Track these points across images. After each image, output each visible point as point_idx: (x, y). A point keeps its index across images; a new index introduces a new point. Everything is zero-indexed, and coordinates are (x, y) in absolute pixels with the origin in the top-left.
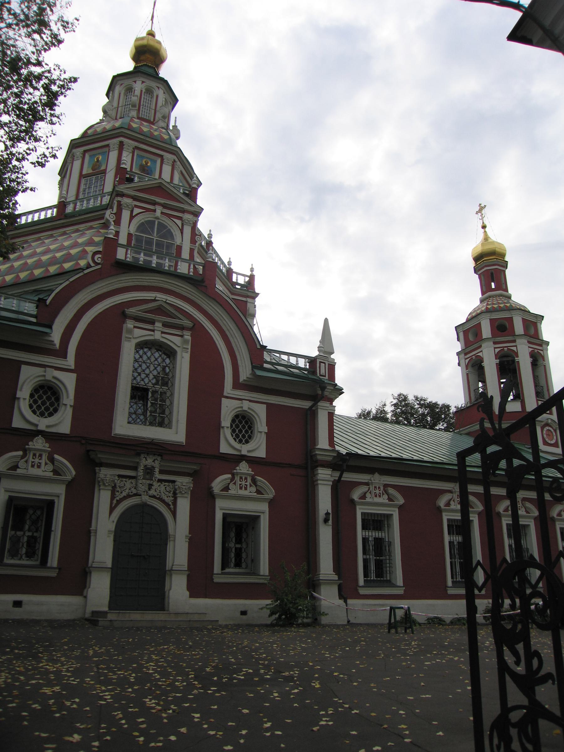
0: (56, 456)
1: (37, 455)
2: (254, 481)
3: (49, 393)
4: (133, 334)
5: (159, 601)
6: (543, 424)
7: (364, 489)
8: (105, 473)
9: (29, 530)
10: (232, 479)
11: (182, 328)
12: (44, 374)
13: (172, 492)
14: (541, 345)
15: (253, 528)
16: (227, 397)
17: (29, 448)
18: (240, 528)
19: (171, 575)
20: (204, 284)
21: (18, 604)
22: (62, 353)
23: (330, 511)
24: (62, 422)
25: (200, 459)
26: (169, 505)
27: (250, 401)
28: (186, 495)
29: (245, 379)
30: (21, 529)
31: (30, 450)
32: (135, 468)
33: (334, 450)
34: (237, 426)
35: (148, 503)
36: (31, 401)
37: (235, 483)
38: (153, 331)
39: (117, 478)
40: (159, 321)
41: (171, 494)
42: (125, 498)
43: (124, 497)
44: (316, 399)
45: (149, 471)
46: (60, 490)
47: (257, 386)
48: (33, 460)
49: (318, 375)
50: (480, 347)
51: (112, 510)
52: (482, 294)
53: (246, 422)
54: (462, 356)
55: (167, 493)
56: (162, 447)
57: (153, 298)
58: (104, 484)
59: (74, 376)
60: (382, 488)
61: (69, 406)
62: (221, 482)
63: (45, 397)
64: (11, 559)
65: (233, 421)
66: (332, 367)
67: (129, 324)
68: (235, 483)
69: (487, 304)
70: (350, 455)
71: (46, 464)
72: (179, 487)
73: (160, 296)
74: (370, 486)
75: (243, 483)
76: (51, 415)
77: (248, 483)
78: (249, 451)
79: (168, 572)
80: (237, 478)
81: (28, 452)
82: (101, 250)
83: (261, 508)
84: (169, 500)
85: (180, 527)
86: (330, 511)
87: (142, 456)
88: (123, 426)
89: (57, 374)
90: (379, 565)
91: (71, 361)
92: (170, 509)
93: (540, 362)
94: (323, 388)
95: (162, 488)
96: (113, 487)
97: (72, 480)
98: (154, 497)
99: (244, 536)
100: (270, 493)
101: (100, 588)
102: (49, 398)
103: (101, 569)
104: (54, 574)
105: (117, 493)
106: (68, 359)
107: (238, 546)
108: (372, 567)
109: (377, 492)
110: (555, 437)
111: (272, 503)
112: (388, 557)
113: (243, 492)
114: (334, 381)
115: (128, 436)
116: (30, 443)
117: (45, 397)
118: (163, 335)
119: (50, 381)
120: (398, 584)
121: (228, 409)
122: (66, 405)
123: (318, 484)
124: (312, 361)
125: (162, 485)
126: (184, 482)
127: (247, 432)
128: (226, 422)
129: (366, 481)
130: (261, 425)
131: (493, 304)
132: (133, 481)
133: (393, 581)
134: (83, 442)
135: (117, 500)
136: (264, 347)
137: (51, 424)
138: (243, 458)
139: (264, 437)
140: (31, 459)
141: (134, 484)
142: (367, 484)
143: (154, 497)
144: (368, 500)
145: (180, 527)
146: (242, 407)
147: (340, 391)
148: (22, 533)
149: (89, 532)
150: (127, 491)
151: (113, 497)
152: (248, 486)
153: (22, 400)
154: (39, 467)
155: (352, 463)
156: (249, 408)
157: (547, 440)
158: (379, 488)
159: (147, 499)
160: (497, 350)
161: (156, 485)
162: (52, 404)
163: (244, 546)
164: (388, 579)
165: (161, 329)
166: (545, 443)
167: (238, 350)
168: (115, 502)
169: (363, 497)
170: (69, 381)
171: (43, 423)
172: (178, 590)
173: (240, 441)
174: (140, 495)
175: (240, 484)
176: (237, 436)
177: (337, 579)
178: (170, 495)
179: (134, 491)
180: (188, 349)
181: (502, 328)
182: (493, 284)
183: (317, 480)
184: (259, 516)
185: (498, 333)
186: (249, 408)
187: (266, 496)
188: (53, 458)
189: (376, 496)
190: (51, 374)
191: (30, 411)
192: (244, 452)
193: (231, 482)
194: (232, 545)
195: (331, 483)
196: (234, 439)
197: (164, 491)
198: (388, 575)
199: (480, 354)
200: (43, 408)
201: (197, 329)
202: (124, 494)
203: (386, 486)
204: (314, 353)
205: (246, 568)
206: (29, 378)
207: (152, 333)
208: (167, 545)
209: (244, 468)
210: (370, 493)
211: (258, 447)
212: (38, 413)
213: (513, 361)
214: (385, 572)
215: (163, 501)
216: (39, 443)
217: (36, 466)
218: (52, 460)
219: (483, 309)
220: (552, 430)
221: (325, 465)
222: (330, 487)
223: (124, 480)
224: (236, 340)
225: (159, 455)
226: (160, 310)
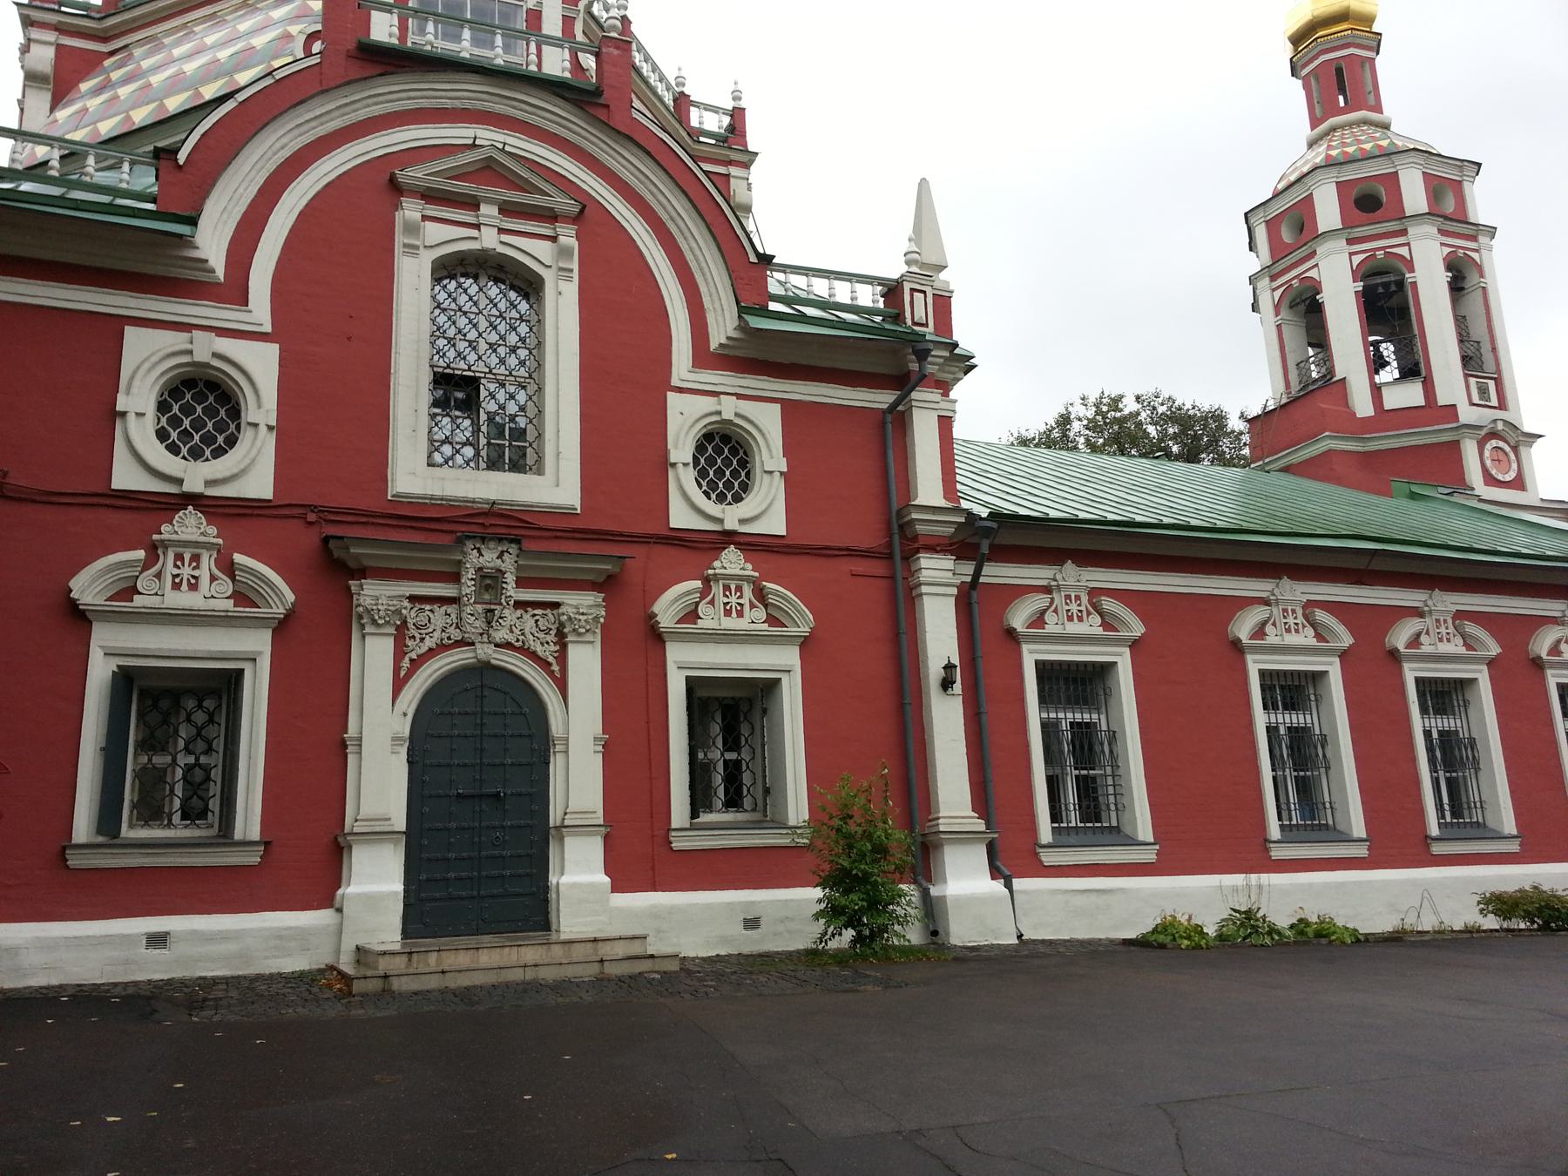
0: (239, 558)
1: (187, 557)
3: (211, 399)
4: (424, 238)
5: (530, 909)
6: (1483, 433)
7: (1039, 601)
8: (374, 594)
9: (188, 751)
10: (706, 591)
11: (551, 217)
12: (189, 347)
13: (553, 632)
14: (1474, 238)
15: (765, 711)
16: (680, 390)
17: (162, 541)
18: (731, 710)
19: (561, 839)
20: (601, 101)
21: (158, 940)
22: (235, 291)
23: (956, 661)
24: (251, 468)
25: (614, 551)
26: (550, 664)
27: (739, 396)
28: (589, 637)
29: (724, 341)
30: (162, 748)
31: (165, 545)
32: (455, 578)
33: (957, 510)
34: (711, 462)
36: (164, 420)
37: (712, 602)
38: (477, 227)
39: (406, 603)
40: (490, 201)
42: (431, 653)
44: (903, 383)
45: (490, 582)
47: (761, 354)
48: (176, 571)
49: (909, 322)
50: (1314, 253)
51: (398, 685)
52: (1313, 127)
53: (734, 451)
54: (1264, 283)
55: (541, 635)
57: (470, 142)
58: (374, 622)
59: (272, 351)
60: (1085, 599)
61: (263, 429)
62: (676, 600)
63: (199, 409)
65: (700, 449)
66: (943, 304)
67: (411, 210)
68: (712, 602)
69: (1330, 147)
70: (995, 515)
71: (213, 578)
72: (570, 618)
73: (487, 136)
74: (1055, 595)
75: (733, 600)
76: (219, 453)
77: (744, 601)
78: (742, 521)
79: (552, 832)
80: (718, 589)
81: (160, 552)
82: (319, 27)
83: (781, 661)
84: (548, 651)
86: (956, 661)
88: (413, 472)
89: (226, 345)
90: (1087, 789)
91: (260, 310)
92: (551, 674)
93: (1472, 279)
94: (922, 355)
96: (398, 628)
97: (287, 616)
98: (508, 645)
99: (745, 730)
100: (803, 622)
101: (377, 880)
102: (211, 412)
103: (378, 836)
104: (253, 858)
105: (410, 643)
106: (251, 306)
107: (731, 756)
108: (1071, 795)
109: (1074, 607)
110: (1515, 466)
112: (1109, 769)
113: (732, 623)
114: (951, 337)
115: (432, 498)
116: (165, 528)
117: (199, 409)
119: (207, 365)
120: (1141, 838)
121: (684, 420)
122: (256, 425)
124: (892, 291)
125: (527, 617)
126: (582, 604)
127: (735, 474)
128: (681, 449)
129: (1044, 583)
130: (771, 456)
131: (1344, 144)
132: (452, 609)
133: (1127, 829)
134: (312, 517)
135: (412, 660)
136: (766, 260)
137: (219, 476)
138: (728, 538)
139: (779, 485)
140: (170, 569)
141: (453, 616)
142: (1047, 590)
143: (508, 645)
144: (1052, 627)
146: (719, 413)
147: (965, 364)
148: (169, 759)
149: (343, 745)
150: (437, 635)
151: (400, 653)
152: (747, 607)
153: (131, 417)
154: (193, 587)
155: (1006, 539)
156: (737, 415)
157: (1493, 472)
158: (1078, 598)
160: (1357, 259)
161: (510, 615)
162: (220, 427)
163: (745, 755)
164: (1114, 823)
165: (496, 222)
166: (1490, 480)
167: (701, 269)
168: (406, 663)
169: (1039, 620)
170: (259, 368)
171: (196, 476)
172: (578, 871)
173: (721, 498)
174: (473, 644)
175: (175, 576)
176: (713, 485)
177: (982, 828)
178: (549, 638)
179: (456, 635)
180: (571, 271)
181: (1369, 203)
182: (1341, 98)
185: (1370, 241)
186: (737, 415)
187: (792, 630)
188: (232, 563)
189: (1070, 619)
190: (204, 348)
191: (161, 448)
192: (731, 524)
193: (702, 598)
194: (716, 754)
195: (955, 591)
196: (705, 493)
197: (534, 630)
198: (1113, 814)
199: (1313, 273)
200: (197, 437)
201: (586, 215)
202: (429, 643)
203: (1094, 593)
204: (894, 269)
205: (754, 810)
206: (146, 361)
207: (474, 233)
209: (731, 562)
210: (1056, 611)
211: (765, 509)
212: (184, 451)
213: (1401, 284)
214: (1103, 807)
215: (533, 656)
217: (185, 586)
218: (229, 569)
219: (1317, 160)
220: (1507, 449)
221: (935, 547)
225: (512, 541)
226: (490, 170)
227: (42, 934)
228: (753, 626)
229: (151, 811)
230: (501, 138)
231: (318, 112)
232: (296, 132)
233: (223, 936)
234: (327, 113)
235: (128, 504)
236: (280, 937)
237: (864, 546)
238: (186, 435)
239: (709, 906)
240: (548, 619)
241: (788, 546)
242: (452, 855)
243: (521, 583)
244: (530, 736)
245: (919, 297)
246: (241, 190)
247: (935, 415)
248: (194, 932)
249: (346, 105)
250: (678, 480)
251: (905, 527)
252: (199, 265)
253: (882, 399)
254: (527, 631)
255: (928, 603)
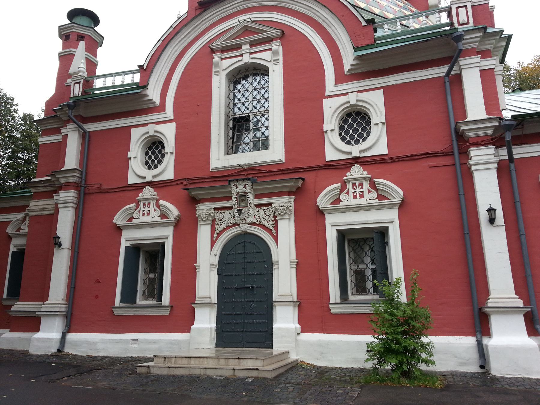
2: (373, 185)
5: (264, 338)
8: (203, 209)
11: (269, 40)
13: (272, 216)
16: (330, 97)
17: (347, 179)
18: (364, 244)
21: (135, 342)
22: (162, 108)
24: (167, 170)
31: (348, 181)
35: (248, 231)
36: (147, 157)
38: (241, 55)
39: (213, 211)
40: (245, 43)
41: (271, 218)
42: (225, 229)
43: (224, 228)
44: (451, 59)
46: (168, 232)
47: (370, 68)
48: (354, 191)
55: (267, 218)
56: (255, 169)
61: (380, 125)
64: (152, 300)
67: (216, 58)
68: (348, 193)
73: (242, 18)
78: (361, 151)
80: (350, 186)
83: (389, 218)
85: (284, 251)
87: (232, 184)
92: (272, 234)
95: (262, 213)
100: (397, 194)
101: (206, 321)
104: (167, 312)
111: (402, 206)
116: (140, 195)
118: (252, 56)
119: (153, 136)
121: (331, 111)
123: (472, 171)
132: (230, 211)
135: (218, 233)
138: (356, 160)
140: (351, 191)
141: (232, 214)
145: (284, 251)
151: (213, 230)
154: (362, 196)
159: (246, 227)
161: (253, 211)
165: (248, 51)
168: (215, 235)
171: (355, 151)
172: (285, 321)
174: (239, 225)
176: (361, 135)
178: (270, 219)
183: (471, 166)
184: (387, 228)
187: (392, 201)
188: (374, 182)
190: (151, 130)
195: (496, 165)
201: (285, 34)
202: (223, 226)
207: (240, 58)
208: (272, 274)
211: (377, 143)
212: (353, 142)
215: (264, 227)
216: (148, 192)
217: (146, 214)
221: (480, 143)
222: (495, 171)
223: (222, 211)
224: (333, 28)
226: (246, 30)
227: (103, 338)
228: (370, 202)
229: (361, 289)
230: (248, 17)
231: (185, 34)
232: (179, 44)
233: (155, 342)
234: (189, 33)
235: (134, 188)
236: (171, 343)
237: (436, 151)
238: (352, 137)
239: (348, 343)
240: (269, 211)
241: (389, 159)
242: (234, 313)
243: (257, 196)
244: (264, 262)
245: (462, 11)
246: (163, 71)
247: (478, 70)
248: (145, 340)
249: (195, 27)
250: (328, 138)
251: (460, 136)
252: (149, 102)
253: (441, 71)
254: (261, 217)
255: (477, 176)
